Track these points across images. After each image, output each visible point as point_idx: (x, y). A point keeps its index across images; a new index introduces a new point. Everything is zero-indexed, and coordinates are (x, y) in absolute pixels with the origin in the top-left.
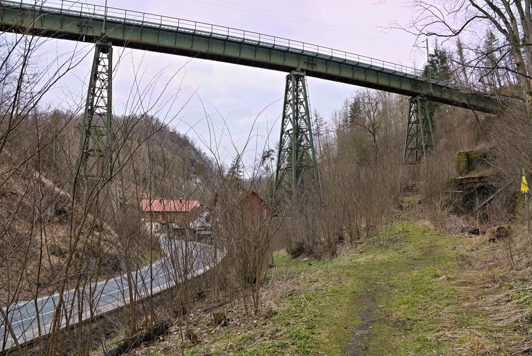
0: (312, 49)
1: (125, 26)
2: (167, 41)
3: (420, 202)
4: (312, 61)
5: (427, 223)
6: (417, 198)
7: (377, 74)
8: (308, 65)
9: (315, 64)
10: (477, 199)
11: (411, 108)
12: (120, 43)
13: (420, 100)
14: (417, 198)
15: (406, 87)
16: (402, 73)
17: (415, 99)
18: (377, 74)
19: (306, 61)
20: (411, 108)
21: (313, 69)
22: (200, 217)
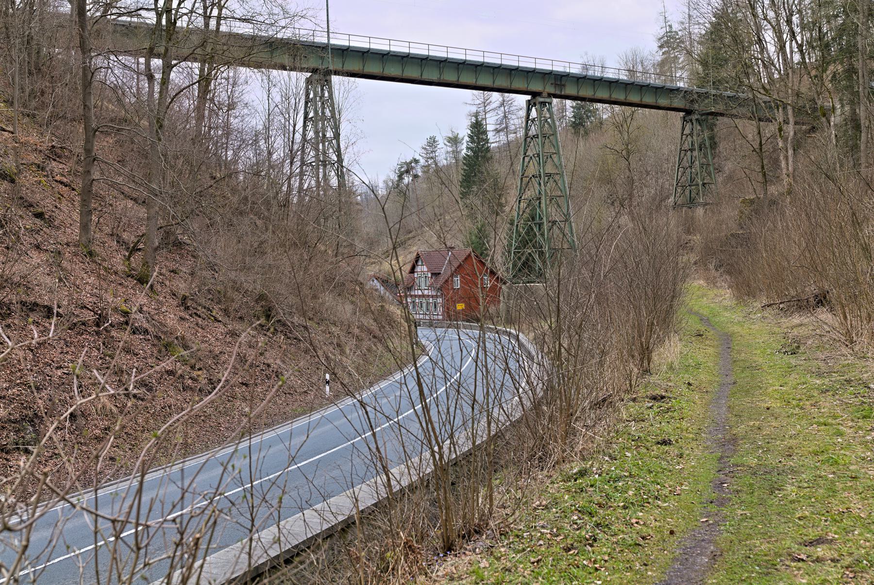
0: (559, 68)
1: (344, 52)
2: (392, 69)
3: (695, 263)
4: (561, 80)
5: (702, 282)
6: (693, 257)
7: (510, 74)
8: (555, 87)
9: (564, 85)
10: (62, 9)
11: (683, 129)
12: (336, 73)
13: (697, 120)
14: (693, 257)
15: (678, 103)
16: (565, 72)
17: (690, 117)
18: (510, 74)
19: (553, 81)
20: (683, 129)
21: (561, 92)
22: (637, 411)
